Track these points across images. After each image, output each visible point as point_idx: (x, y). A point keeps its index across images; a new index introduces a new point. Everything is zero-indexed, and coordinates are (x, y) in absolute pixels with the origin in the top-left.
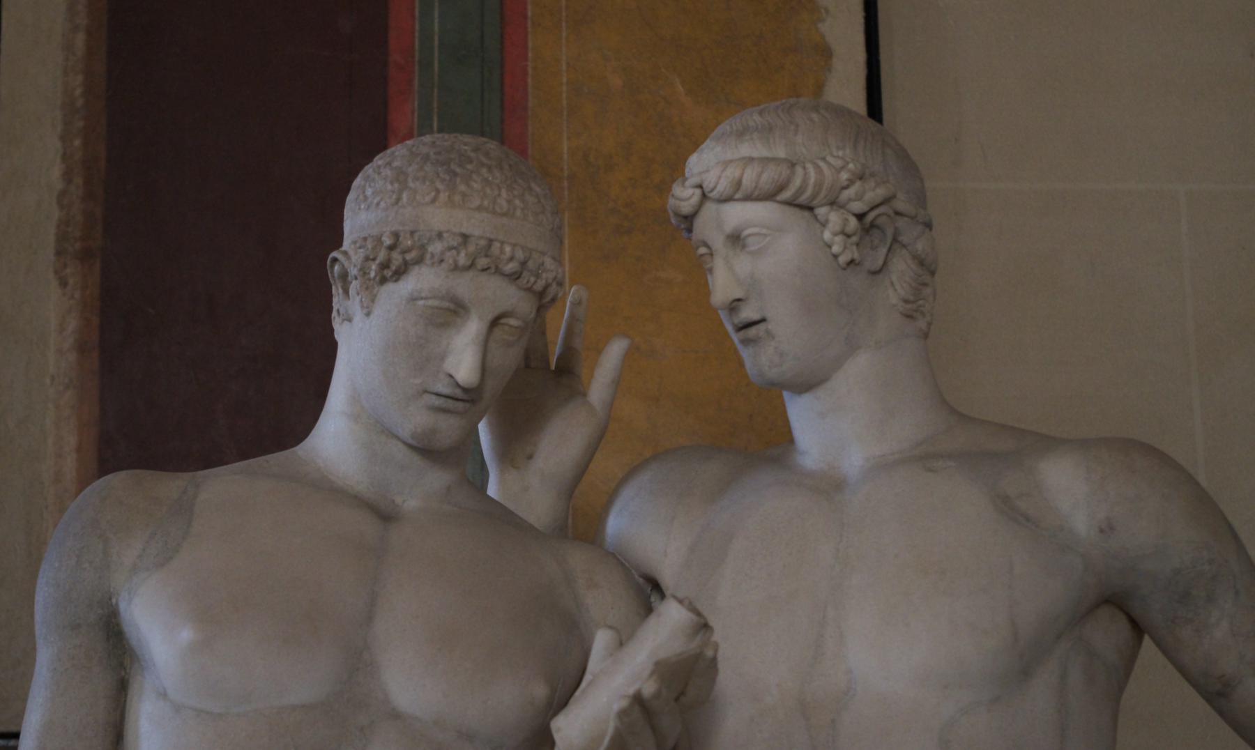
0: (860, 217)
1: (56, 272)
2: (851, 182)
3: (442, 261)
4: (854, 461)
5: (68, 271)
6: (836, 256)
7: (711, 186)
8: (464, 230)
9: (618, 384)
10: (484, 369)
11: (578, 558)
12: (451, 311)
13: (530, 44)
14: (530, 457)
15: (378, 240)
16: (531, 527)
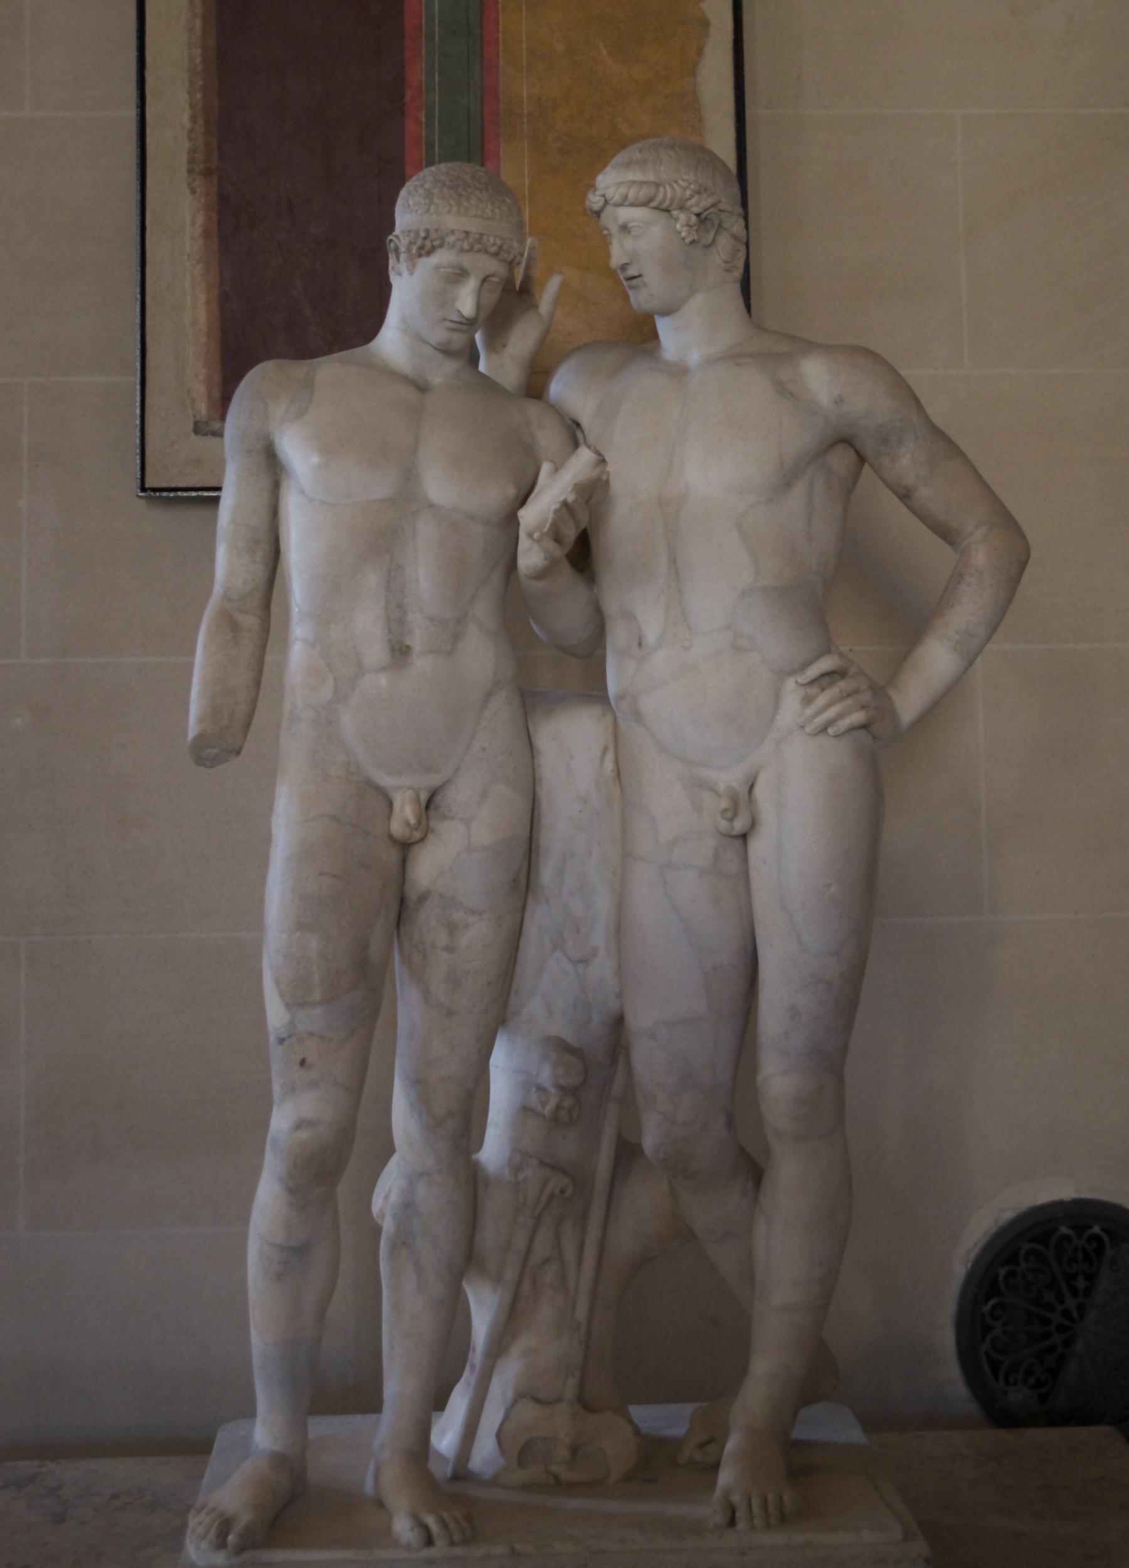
0: (698, 215)
1: (189, 184)
2: (692, 196)
4: (694, 357)
5: (197, 183)
6: (683, 239)
8: (467, 229)
9: (557, 302)
10: (478, 306)
11: (533, 409)
12: (460, 275)
13: (501, 21)
14: (504, 346)
15: (417, 233)
16: (506, 391)
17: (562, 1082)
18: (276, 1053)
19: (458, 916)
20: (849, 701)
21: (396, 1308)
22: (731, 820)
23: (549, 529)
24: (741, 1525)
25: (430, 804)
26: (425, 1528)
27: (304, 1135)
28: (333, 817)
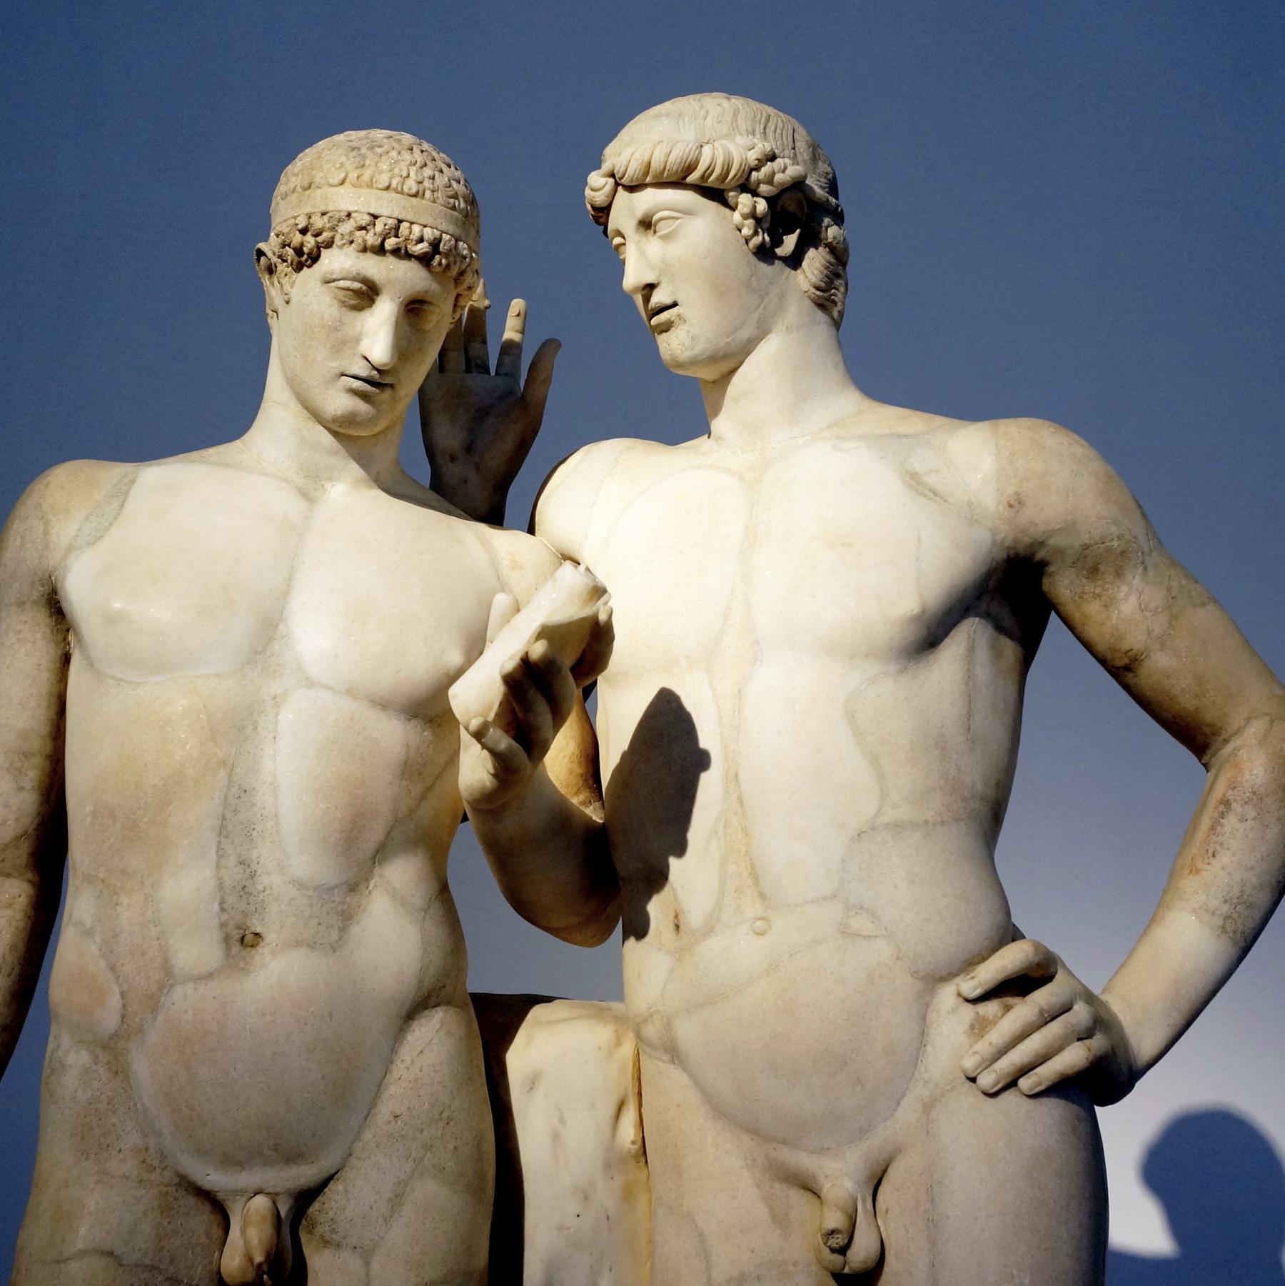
3: (352, 242)
7: (622, 170)
12: (366, 294)
23: (497, 715)
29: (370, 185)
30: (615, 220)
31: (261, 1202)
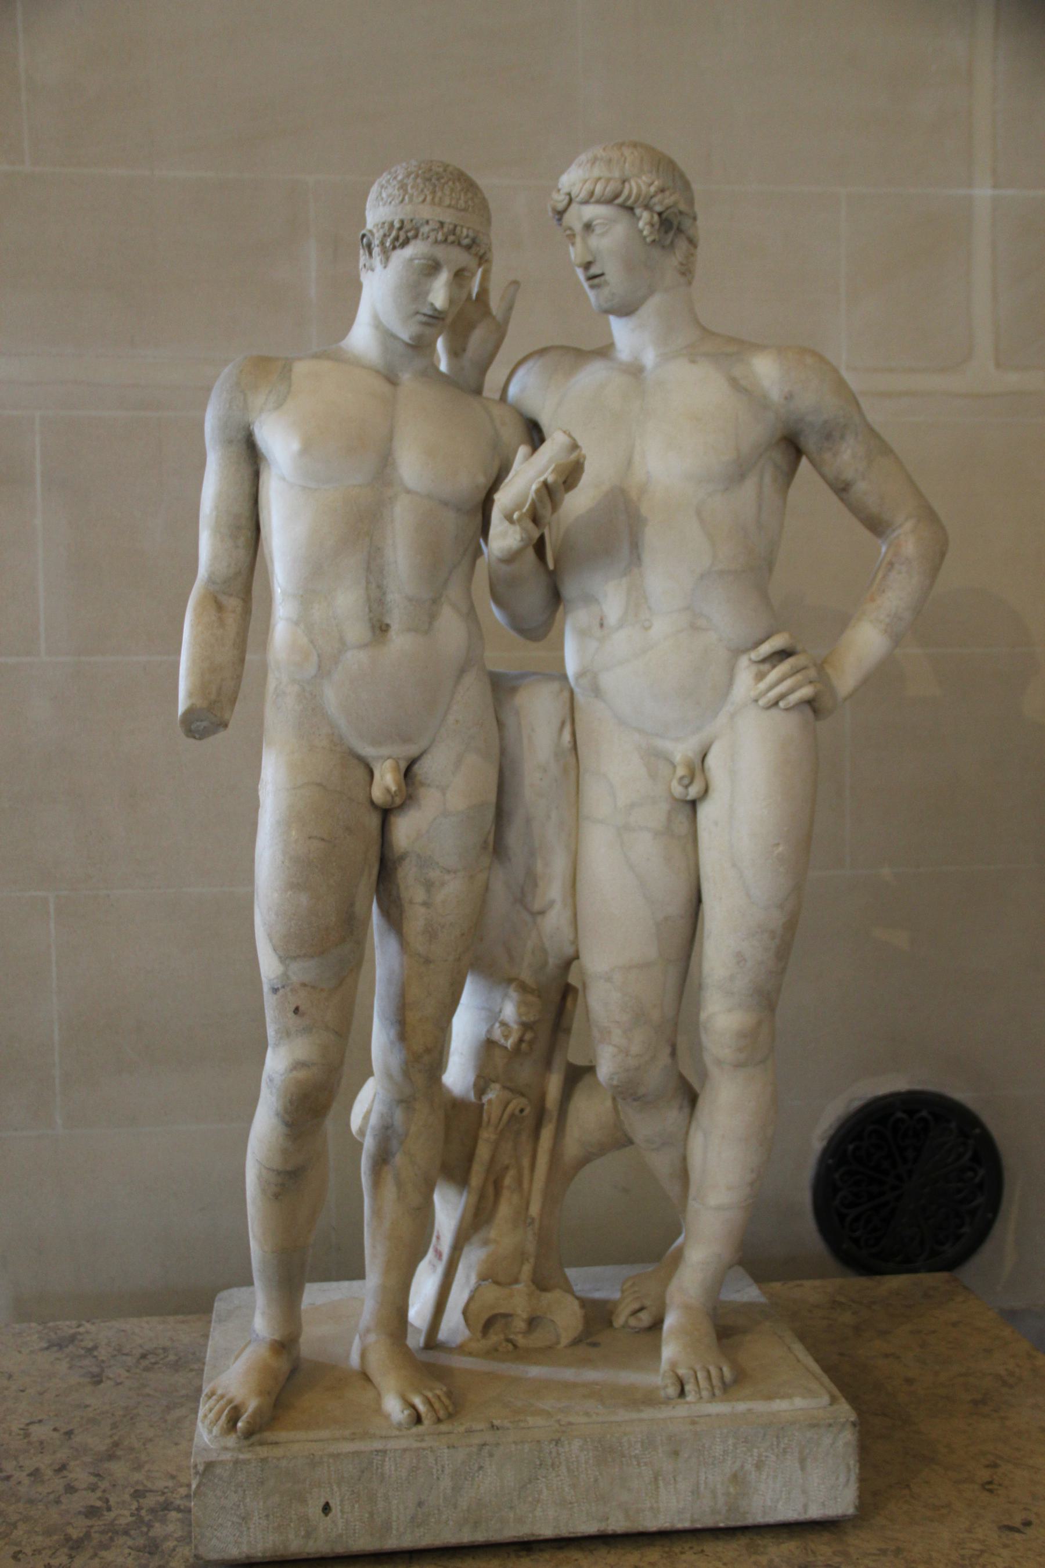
0: (660, 214)
8: (441, 219)
12: (433, 268)
15: (392, 225)
17: (524, 1019)
18: (270, 1002)
19: (434, 874)
20: (799, 677)
21: (377, 1212)
22: (687, 787)
24: (690, 1397)
25: (408, 773)
26: (413, 1407)
27: (301, 1074)
28: (319, 785)
29: (440, 204)
30: (570, 218)
31: (389, 763)
